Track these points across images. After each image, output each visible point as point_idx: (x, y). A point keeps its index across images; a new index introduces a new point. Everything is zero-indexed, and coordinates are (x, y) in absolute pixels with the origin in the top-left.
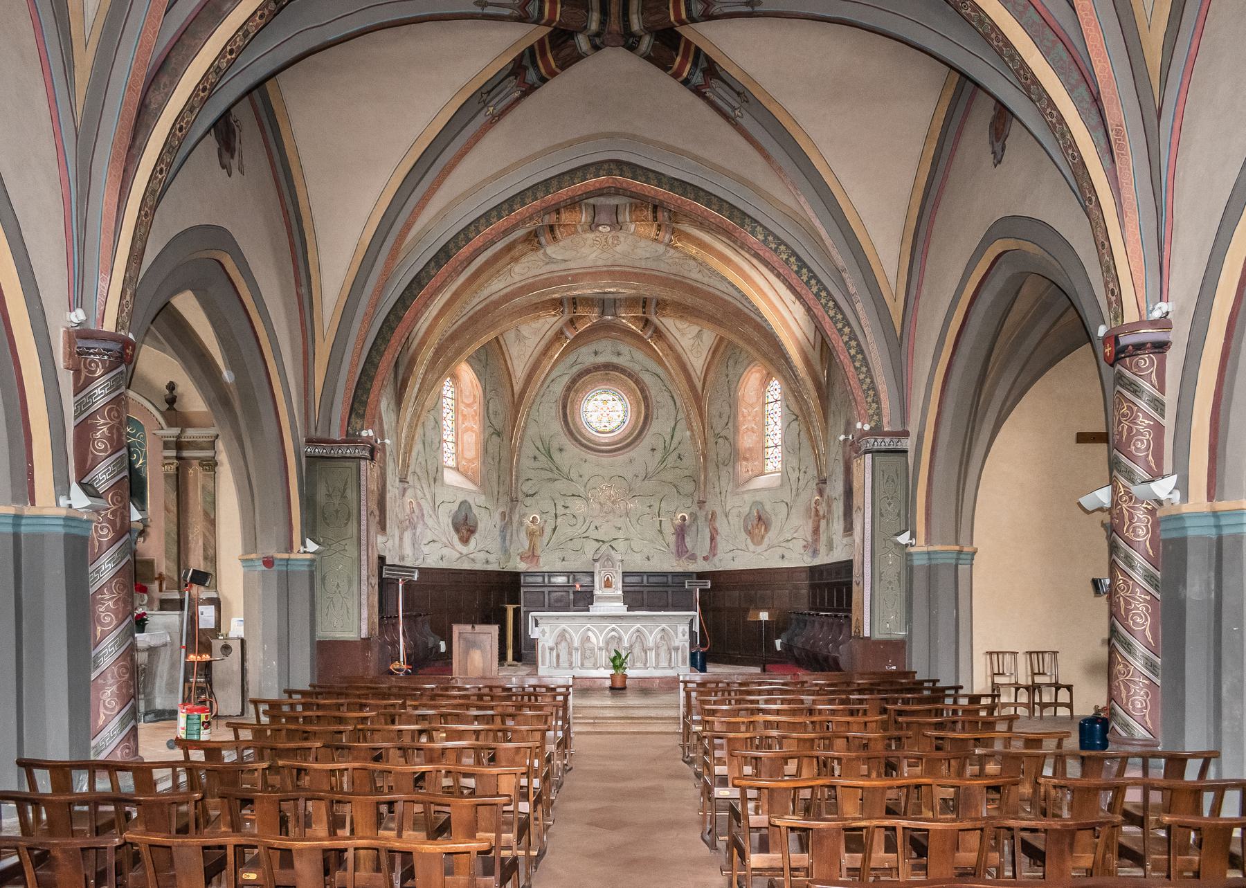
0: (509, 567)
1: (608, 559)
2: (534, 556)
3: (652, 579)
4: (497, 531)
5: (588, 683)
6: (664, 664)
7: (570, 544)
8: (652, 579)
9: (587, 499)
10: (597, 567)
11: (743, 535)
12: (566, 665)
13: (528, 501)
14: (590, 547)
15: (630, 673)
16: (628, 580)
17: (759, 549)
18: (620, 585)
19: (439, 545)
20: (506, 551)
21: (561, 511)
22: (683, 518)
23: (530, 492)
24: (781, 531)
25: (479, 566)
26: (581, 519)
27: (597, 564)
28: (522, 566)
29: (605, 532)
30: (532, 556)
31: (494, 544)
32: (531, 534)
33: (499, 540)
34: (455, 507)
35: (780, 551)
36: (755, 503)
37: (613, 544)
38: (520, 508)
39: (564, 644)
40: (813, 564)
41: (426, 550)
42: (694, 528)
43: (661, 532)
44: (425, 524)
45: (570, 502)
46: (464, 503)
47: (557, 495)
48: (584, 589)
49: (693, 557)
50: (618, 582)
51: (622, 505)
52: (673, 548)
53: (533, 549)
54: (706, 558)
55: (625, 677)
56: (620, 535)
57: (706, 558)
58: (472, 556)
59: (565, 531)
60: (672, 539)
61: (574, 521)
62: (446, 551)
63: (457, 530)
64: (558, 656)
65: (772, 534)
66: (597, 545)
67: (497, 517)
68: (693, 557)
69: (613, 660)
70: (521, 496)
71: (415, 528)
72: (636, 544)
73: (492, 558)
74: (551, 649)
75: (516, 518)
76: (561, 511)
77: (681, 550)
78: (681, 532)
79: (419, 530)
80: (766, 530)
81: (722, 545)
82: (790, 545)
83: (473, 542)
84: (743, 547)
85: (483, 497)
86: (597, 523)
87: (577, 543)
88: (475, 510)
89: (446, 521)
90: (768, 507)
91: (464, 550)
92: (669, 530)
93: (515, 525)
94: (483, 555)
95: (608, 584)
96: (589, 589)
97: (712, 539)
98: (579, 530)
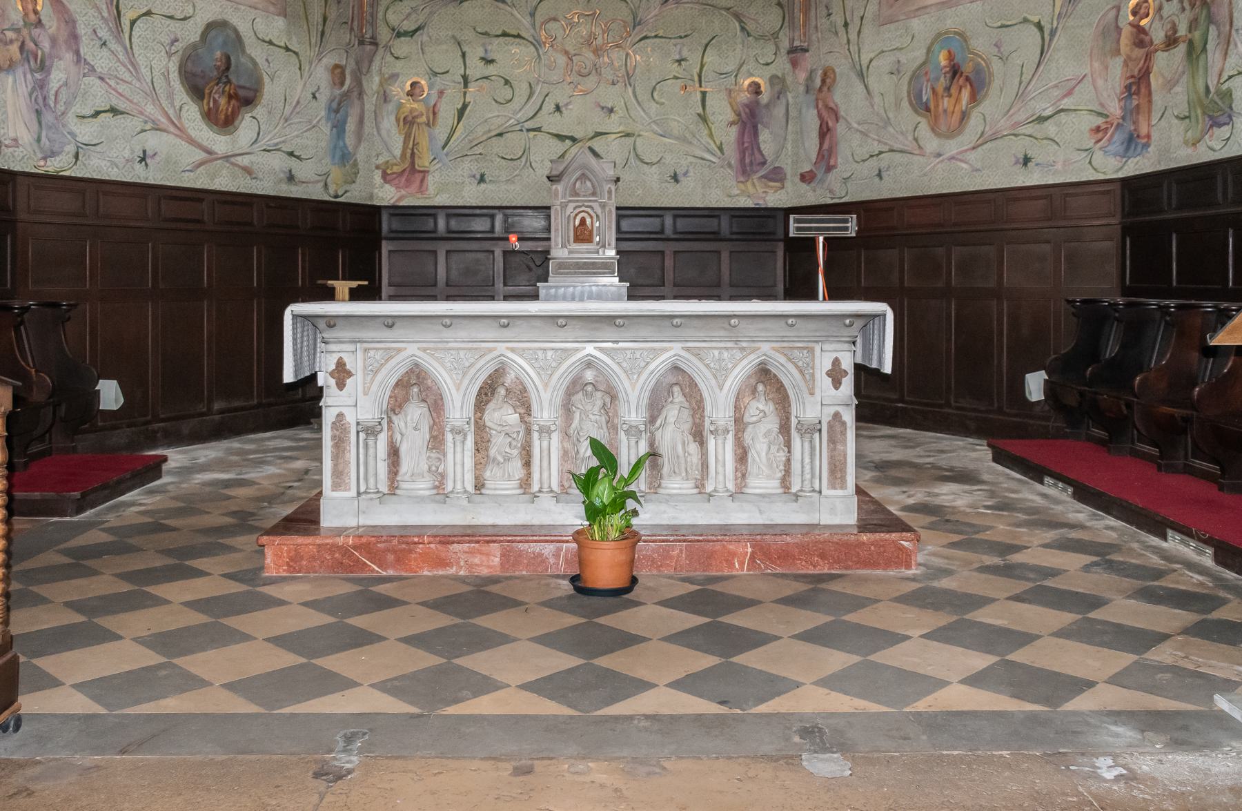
0: (355, 195)
1: (583, 177)
2: (413, 169)
3: (682, 224)
4: (320, 110)
5: (489, 562)
6: (763, 481)
7: (498, 146)
8: (682, 224)
9: (537, 44)
10: (558, 195)
11: (907, 116)
12: (423, 486)
13: (403, 47)
14: (544, 152)
15: (649, 516)
16: (626, 224)
17: (952, 147)
18: (612, 236)
19: (132, 124)
20: (344, 157)
21: (476, 69)
22: (756, 90)
23: (408, 26)
24: (1020, 95)
25: (265, 186)
26: (522, 89)
27: (559, 187)
28: (386, 195)
29: (579, 116)
30: (412, 172)
31: (313, 140)
32: (408, 122)
33: (326, 129)
34: (191, 33)
35: (1019, 146)
36: (941, 38)
37: (597, 144)
38: (381, 64)
39: (415, 412)
40: (1202, 154)
41: (86, 131)
42: (779, 111)
43: (703, 118)
44: (79, 58)
45: (497, 48)
46: (214, 27)
47: (468, 35)
48: (528, 246)
49: (776, 176)
50: (605, 227)
51: (617, 57)
52: (732, 153)
53: (411, 154)
54: (806, 178)
55: (630, 536)
56: (613, 124)
57: (806, 178)
58: (244, 161)
59: (487, 113)
60: (729, 136)
61: (508, 93)
62: (153, 141)
63: (197, 91)
64: (394, 454)
65: (992, 107)
66: (559, 147)
67: (321, 75)
68: (776, 176)
69: (587, 483)
70: (384, 35)
71: (43, 67)
72: (649, 145)
73: (304, 171)
74: (371, 431)
75: (372, 84)
76: (476, 69)
77: (749, 160)
78: (750, 119)
79: (56, 77)
80: (974, 98)
81: (849, 145)
82: (1050, 128)
83: (246, 127)
84: (909, 144)
85: (280, 22)
86: (558, 96)
87: (515, 142)
88: (256, 51)
89: (160, 66)
90: (981, 44)
91: (220, 143)
92: (722, 112)
93: (370, 102)
94: (277, 162)
95: (583, 234)
96: (540, 246)
97: (824, 132)
98: (519, 111)
